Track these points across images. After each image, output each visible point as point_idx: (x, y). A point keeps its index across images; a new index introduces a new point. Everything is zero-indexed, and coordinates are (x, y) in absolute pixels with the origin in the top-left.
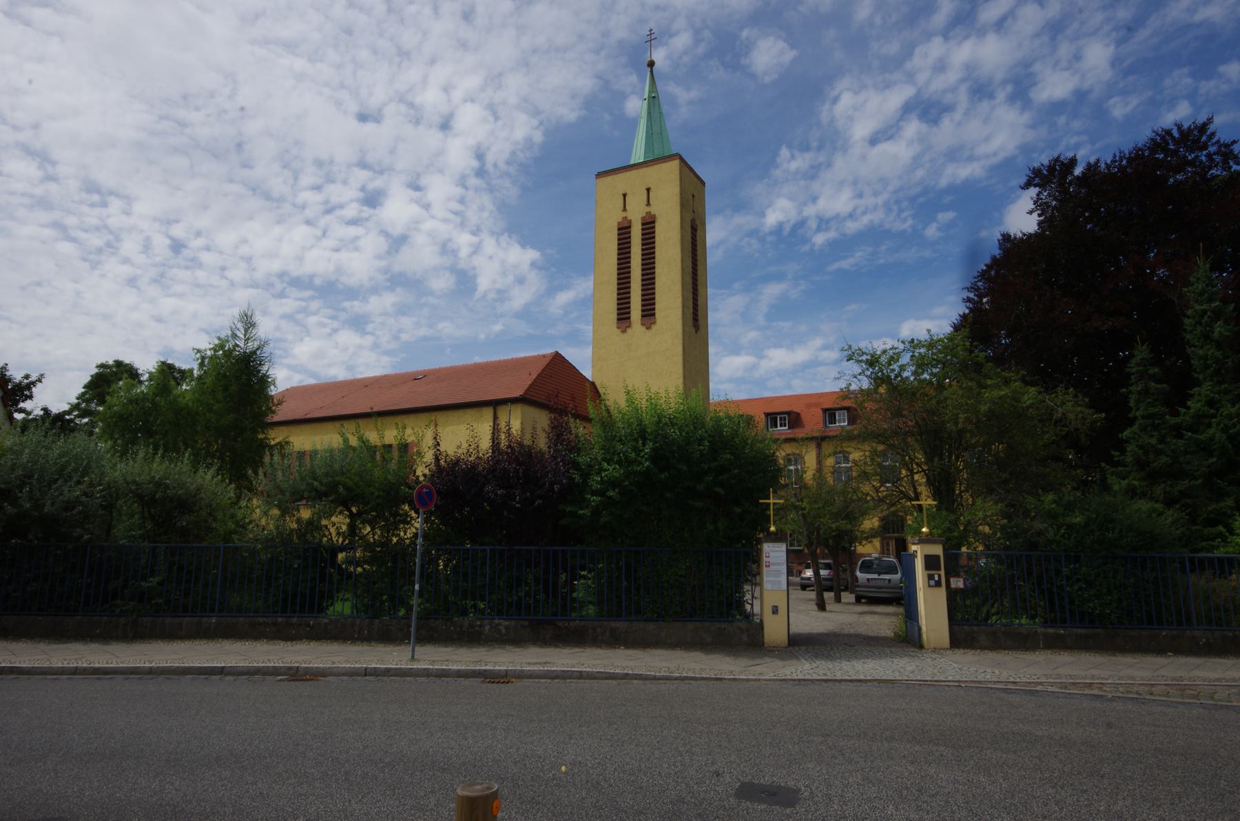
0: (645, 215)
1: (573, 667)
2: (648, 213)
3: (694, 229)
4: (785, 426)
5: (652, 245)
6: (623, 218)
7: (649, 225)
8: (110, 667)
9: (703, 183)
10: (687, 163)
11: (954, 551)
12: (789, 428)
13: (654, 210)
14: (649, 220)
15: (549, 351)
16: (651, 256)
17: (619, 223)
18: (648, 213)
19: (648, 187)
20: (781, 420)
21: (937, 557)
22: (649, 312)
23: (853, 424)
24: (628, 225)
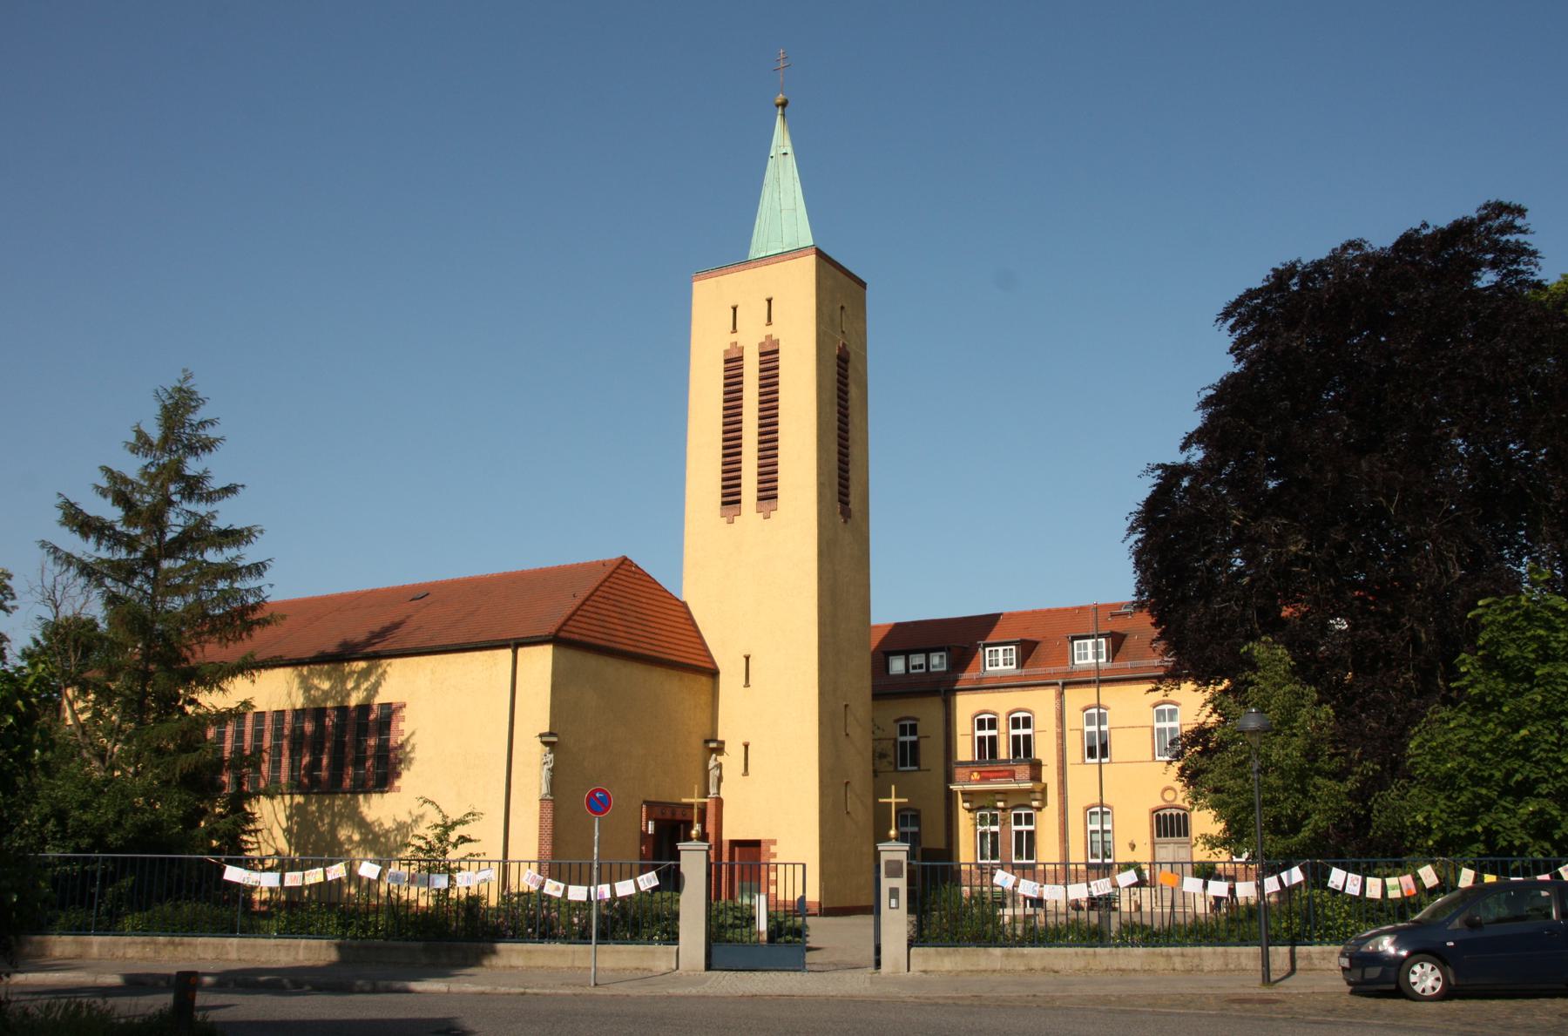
0: (764, 340)
1: (544, 987)
2: (769, 337)
3: (843, 360)
4: (1011, 664)
5: (774, 388)
6: (732, 344)
7: (769, 357)
8: (828, 1001)
9: (863, 284)
10: (830, 258)
11: (595, 858)
12: (1017, 667)
13: (775, 331)
14: (769, 349)
15: (612, 553)
16: (730, 412)
17: (726, 352)
18: (769, 337)
19: (768, 296)
20: (1079, 649)
21: (899, 863)
22: (768, 494)
23: (1023, 666)
24: (775, 348)
